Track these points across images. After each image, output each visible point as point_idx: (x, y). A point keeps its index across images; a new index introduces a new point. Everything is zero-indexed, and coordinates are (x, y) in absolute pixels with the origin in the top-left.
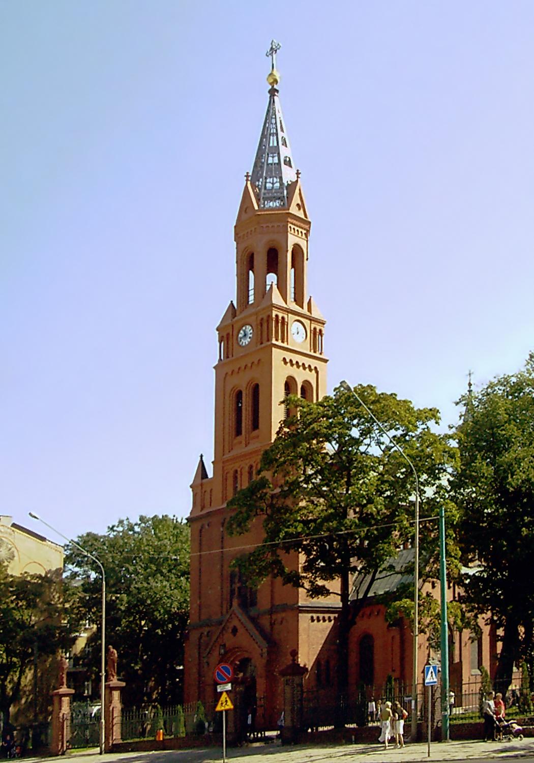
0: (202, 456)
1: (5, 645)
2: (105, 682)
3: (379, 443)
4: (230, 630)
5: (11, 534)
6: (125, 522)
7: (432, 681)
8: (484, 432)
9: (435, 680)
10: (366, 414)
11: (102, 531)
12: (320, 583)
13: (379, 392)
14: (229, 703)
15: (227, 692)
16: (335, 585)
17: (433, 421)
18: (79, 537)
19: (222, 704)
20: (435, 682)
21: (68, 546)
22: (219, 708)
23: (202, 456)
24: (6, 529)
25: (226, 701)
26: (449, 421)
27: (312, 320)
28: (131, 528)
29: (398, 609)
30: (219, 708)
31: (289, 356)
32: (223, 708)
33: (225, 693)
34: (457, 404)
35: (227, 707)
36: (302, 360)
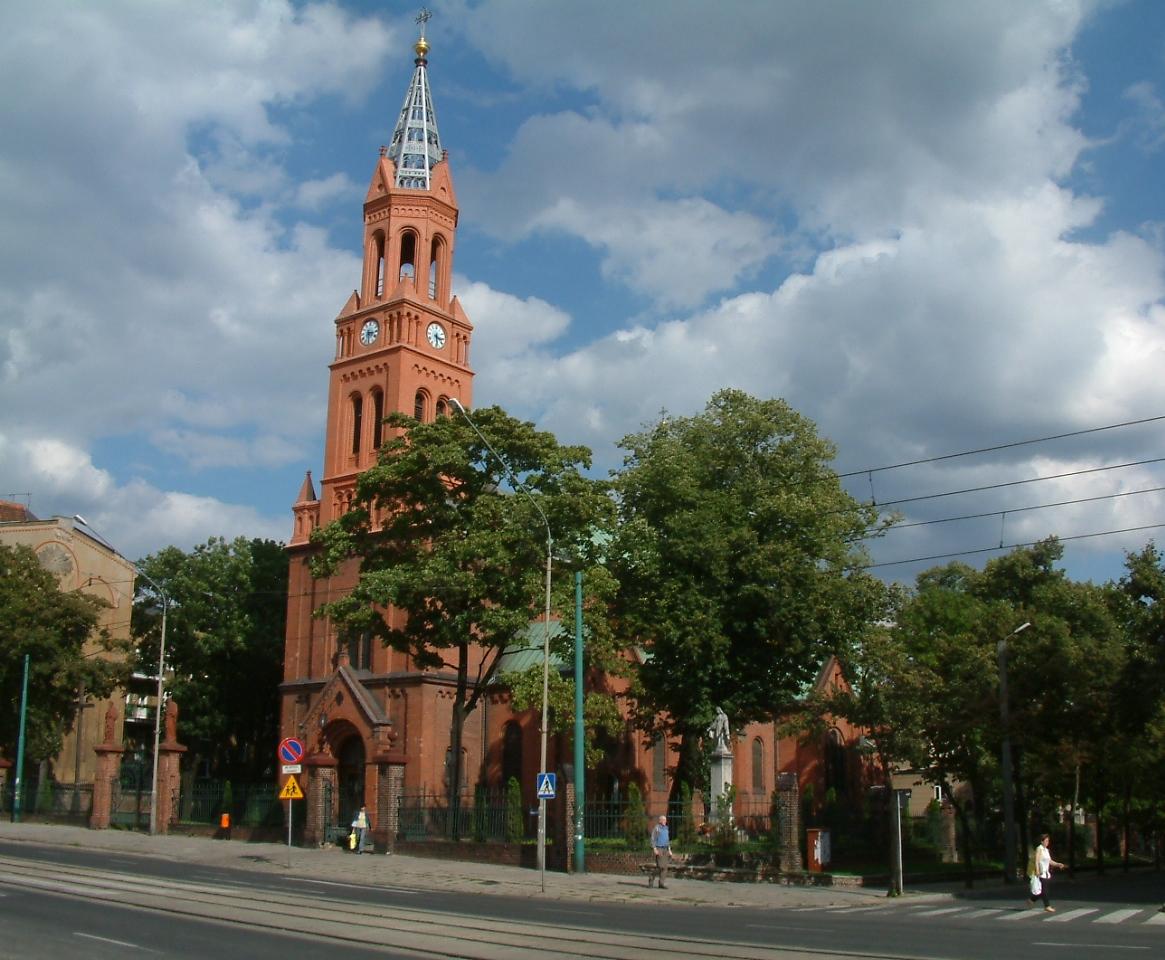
0: (309, 474)
1: (1112, 795)
2: (160, 742)
3: (513, 483)
4: (334, 696)
5: (69, 541)
6: (218, 543)
7: (547, 793)
8: (654, 496)
9: (552, 793)
10: (1034, 640)
12: (430, 649)
13: (508, 417)
14: (298, 790)
15: (294, 775)
16: (450, 655)
17: (581, 464)
19: (288, 790)
20: (552, 796)
21: (144, 562)
22: (283, 795)
23: (309, 474)
24: (63, 533)
25: (294, 787)
26: (608, 465)
27: (454, 323)
28: (225, 550)
30: (283, 795)
31: (422, 363)
32: (289, 796)
33: (292, 777)
34: (620, 446)
35: (294, 796)
36: (439, 369)
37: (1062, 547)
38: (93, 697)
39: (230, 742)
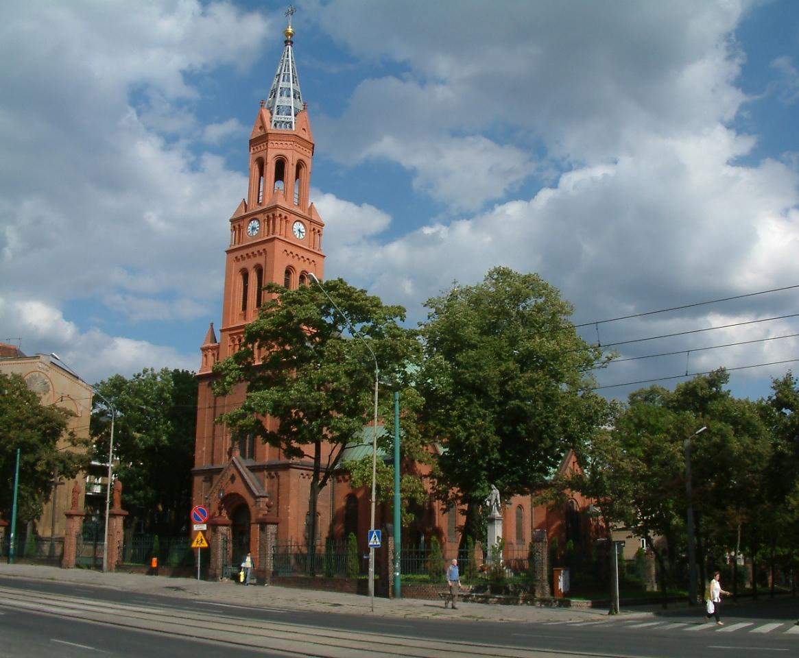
0: (212, 325)
2: (110, 509)
3: (352, 331)
5: (47, 371)
6: (150, 372)
7: (375, 543)
9: (379, 543)
11: (129, 377)
12: (295, 445)
13: (349, 285)
14: (204, 542)
16: (309, 449)
17: (399, 318)
18: (728, 375)
19: (197, 541)
20: (378, 545)
21: (99, 385)
22: (194, 545)
23: (212, 325)
24: (44, 366)
25: (202, 540)
26: (417, 318)
27: (311, 221)
28: (154, 377)
29: (464, 421)
30: (194, 545)
31: (290, 249)
32: (198, 546)
33: (200, 533)
34: (425, 306)
35: (202, 546)
36: (301, 253)
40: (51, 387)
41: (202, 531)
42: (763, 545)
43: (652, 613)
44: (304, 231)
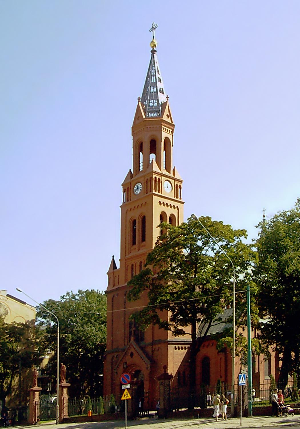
0: (113, 256)
2: (59, 383)
3: (213, 249)
5: (6, 300)
6: (70, 294)
7: (242, 383)
9: (245, 382)
12: (180, 328)
13: (213, 220)
14: (129, 395)
17: (243, 237)
19: (125, 396)
21: (38, 307)
22: (123, 398)
23: (113, 256)
24: (3, 297)
25: (127, 394)
26: (252, 237)
27: (175, 180)
28: (74, 297)
30: (123, 398)
31: (162, 200)
32: (125, 398)
33: (126, 390)
34: (257, 227)
35: (127, 398)
36: (169, 202)
37: (44, 302)
38: (24, 368)
39: (263, 328)
40: (9, 311)
41: (127, 389)
42: (3, 363)
43: (200, 407)
44: (136, 186)
